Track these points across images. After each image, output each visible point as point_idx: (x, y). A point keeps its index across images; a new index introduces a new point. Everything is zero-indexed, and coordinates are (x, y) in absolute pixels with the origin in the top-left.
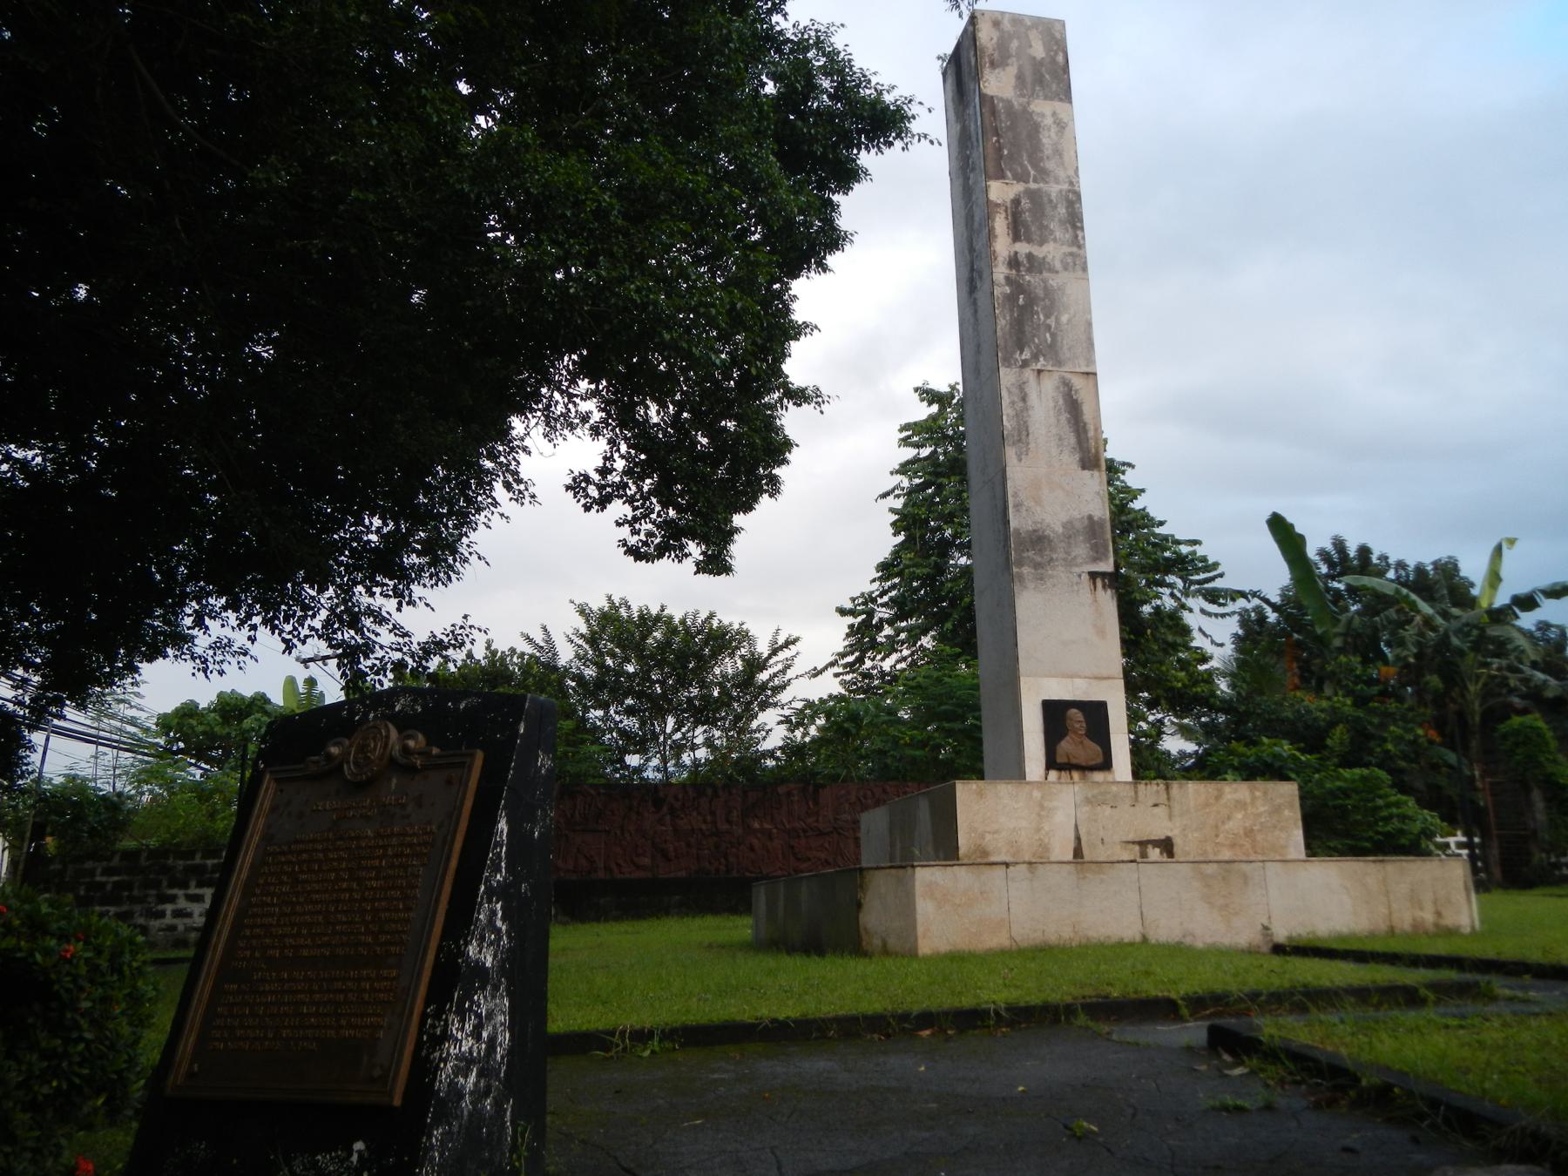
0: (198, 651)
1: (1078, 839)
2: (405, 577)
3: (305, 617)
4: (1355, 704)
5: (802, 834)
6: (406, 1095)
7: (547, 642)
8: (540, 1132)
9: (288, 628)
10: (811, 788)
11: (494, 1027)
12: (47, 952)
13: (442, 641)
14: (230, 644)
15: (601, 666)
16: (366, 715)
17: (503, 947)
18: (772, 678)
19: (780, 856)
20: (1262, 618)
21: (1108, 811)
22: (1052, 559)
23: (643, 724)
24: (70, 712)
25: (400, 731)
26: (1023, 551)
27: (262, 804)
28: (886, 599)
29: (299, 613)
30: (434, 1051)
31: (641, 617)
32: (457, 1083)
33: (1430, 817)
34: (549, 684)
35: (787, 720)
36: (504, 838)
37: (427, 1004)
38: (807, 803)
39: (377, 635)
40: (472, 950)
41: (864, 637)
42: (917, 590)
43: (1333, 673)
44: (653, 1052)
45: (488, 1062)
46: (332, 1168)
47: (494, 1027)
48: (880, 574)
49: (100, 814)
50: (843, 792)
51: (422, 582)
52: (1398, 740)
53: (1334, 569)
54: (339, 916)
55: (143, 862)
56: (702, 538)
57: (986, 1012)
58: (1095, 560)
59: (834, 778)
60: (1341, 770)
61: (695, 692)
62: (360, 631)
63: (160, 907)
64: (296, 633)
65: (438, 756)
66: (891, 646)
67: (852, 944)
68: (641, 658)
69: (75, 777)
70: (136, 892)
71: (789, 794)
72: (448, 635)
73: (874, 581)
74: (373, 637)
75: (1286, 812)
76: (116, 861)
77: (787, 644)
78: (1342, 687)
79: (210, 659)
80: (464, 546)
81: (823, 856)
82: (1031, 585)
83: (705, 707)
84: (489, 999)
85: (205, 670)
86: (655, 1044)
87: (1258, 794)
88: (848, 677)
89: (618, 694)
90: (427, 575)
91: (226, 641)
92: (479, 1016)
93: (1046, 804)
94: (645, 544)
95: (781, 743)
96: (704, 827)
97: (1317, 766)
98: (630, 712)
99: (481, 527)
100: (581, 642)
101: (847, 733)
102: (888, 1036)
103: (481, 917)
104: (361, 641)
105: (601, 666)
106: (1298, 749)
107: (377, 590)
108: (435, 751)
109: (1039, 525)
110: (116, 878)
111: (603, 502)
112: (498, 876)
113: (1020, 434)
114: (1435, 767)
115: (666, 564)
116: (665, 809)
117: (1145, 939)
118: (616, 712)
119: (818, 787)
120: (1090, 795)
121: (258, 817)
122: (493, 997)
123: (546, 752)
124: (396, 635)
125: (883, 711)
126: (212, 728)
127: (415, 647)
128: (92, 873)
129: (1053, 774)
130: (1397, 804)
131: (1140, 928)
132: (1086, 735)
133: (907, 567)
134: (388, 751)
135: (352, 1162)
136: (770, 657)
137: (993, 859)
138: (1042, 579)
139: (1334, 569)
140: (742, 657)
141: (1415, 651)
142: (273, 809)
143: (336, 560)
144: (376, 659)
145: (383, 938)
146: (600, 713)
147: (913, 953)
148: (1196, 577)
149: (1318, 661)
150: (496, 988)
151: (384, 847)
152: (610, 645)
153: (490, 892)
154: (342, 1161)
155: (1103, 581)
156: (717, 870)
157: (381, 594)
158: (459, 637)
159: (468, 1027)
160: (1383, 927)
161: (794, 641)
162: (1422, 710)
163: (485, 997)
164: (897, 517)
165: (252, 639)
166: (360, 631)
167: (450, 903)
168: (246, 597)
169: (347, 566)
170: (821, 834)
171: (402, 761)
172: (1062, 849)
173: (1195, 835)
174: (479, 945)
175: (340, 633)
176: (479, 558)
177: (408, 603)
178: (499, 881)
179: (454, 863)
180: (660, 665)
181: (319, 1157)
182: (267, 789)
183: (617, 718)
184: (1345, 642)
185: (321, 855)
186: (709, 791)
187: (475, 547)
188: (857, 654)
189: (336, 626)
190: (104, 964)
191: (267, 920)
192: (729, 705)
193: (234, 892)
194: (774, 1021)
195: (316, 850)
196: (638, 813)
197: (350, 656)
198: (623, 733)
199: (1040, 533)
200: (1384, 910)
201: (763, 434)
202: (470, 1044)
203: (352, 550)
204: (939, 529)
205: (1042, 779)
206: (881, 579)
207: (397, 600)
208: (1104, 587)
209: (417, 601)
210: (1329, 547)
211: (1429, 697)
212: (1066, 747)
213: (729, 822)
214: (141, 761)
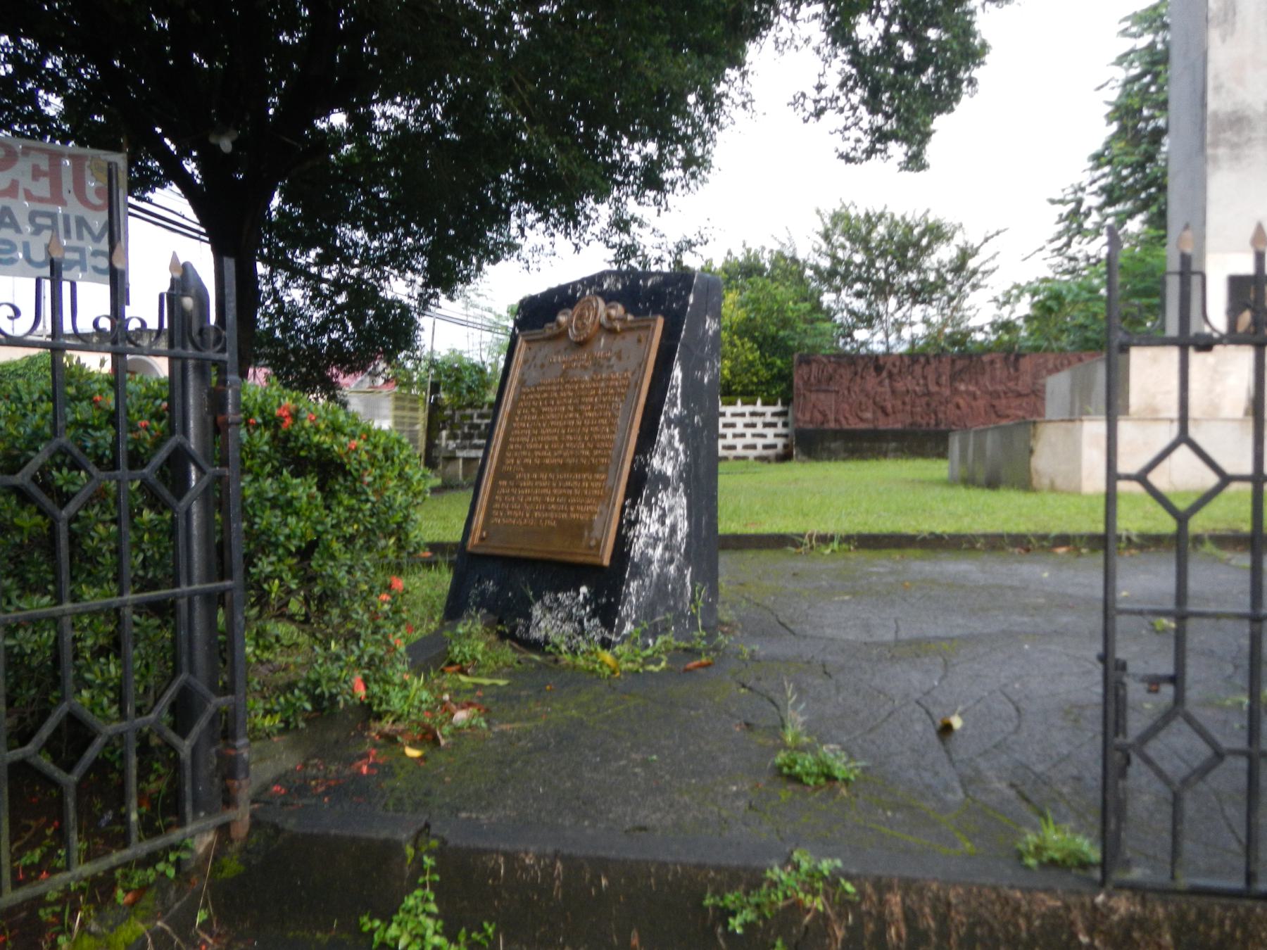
6: (613, 558)
8: (714, 591)
10: (1012, 358)
12: (341, 445)
15: (834, 257)
23: (869, 305)
28: (1095, 187)
35: (996, 300)
37: (626, 499)
41: (1074, 221)
42: (1125, 178)
44: (833, 551)
47: (675, 517)
59: (1037, 349)
65: (632, 322)
67: (1025, 484)
68: (867, 250)
71: (992, 362)
83: (922, 290)
86: (835, 545)
89: (848, 280)
92: (663, 509)
94: (854, 149)
96: (917, 389)
98: (859, 295)
101: (1050, 310)
105: (834, 257)
108: (630, 317)
111: (819, 113)
113: (1226, 14)
116: (884, 374)
119: (1019, 356)
122: (674, 496)
123: (713, 317)
128: (471, 417)
142: (525, 362)
145: (596, 453)
146: (833, 296)
147: (1077, 492)
150: (676, 490)
151: (597, 389)
152: (842, 239)
156: (928, 424)
159: (655, 515)
167: (641, 428)
170: (1019, 395)
171: (607, 325)
180: (883, 254)
186: (922, 360)
190: (379, 453)
191: (523, 439)
192: (943, 287)
194: (932, 534)
196: (862, 377)
198: (852, 313)
201: (962, 39)
204: (1153, 117)
213: (938, 384)
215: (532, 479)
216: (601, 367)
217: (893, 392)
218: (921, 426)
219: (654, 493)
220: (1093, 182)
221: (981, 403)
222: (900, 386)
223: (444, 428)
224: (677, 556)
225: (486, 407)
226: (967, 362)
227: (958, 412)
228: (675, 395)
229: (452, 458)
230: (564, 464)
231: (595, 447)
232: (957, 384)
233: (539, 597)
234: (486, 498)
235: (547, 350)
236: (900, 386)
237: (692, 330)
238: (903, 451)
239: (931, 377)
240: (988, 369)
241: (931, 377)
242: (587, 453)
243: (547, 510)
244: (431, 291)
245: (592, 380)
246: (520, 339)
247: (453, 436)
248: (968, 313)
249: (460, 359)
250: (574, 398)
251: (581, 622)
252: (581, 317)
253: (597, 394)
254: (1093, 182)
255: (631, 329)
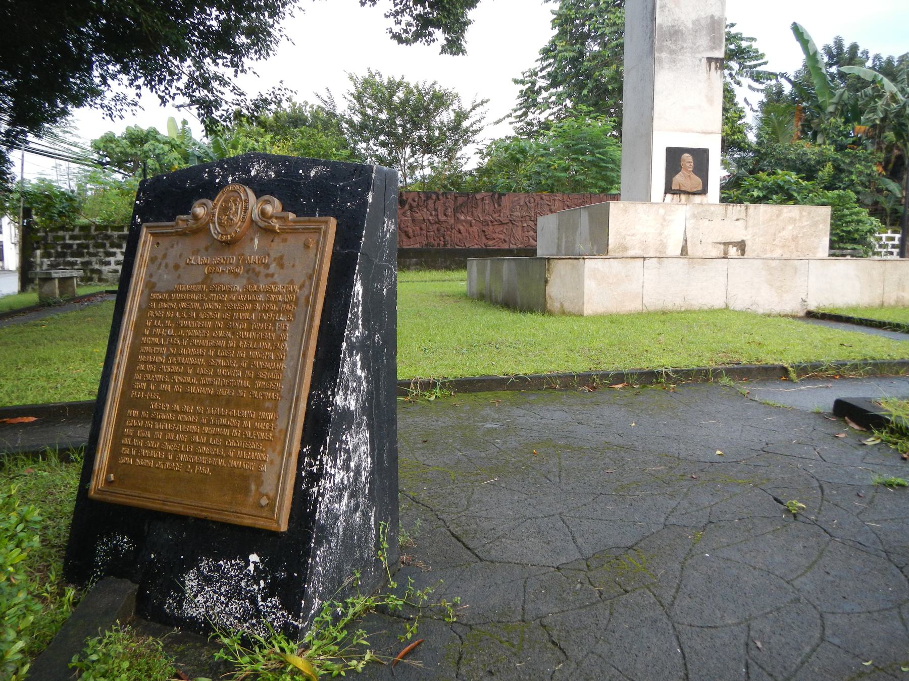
0: (106, 102)
1: (686, 240)
2: (237, 52)
3: (171, 81)
4: (836, 150)
5: (490, 223)
7: (329, 98)
9: (162, 88)
10: (496, 196)
11: (360, 457)
13: (266, 99)
14: (125, 98)
15: (364, 114)
16: (225, 178)
17: (363, 391)
18: (472, 125)
19: (477, 236)
20: (780, 92)
21: (706, 222)
22: (682, 47)
23: (390, 153)
24: (30, 137)
25: (258, 196)
26: (663, 41)
27: (142, 256)
28: (544, 73)
29: (168, 78)
30: (312, 486)
31: (390, 82)
32: (333, 509)
33: (875, 221)
34: (332, 125)
35: (481, 152)
36: (360, 299)
37: (303, 445)
38: (494, 205)
39: (222, 93)
40: (339, 400)
41: (530, 98)
43: (825, 129)
45: (355, 486)
46: (232, 573)
47: (360, 457)
48: (542, 56)
49: (63, 203)
50: (516, 199)
51: (250, 56)
52: (860, 173)
53: (833, 59)
54: (219, 361)
55: (93, 232)
56: (447, 30)
57: (659, 374)
58: (712, 48)
59: (509, 188)
60: (826, 191)
61: (424, 132)
62: (211, 91)
63: (107, 259)
64: (167, 92)
66: (547, 104)
69: (43, 180)
70: (91, 250)
71: (483, 199)
72: (270, 95)
73: (537, 60)
74: (219, 94)
75: (821, 226)
76: (77, 232)
77: (482, 103)
78: (829, 138)
79: (113, 108)
80: (277, 30)
81: (502, 237)
82: (666, 66)
84: (354, 436)
85: (111, 116)
87: (804, 214)
88: (519, 125)
89: (375, 132)
90: (253, 51)
91: (122, 96)
92: (347, 451)
93: (667, 217)
94: (406, 31)
95: (476, 167)
96: (430, 218)
97: (811, 188)
98: (383, 144)
99: (288, 16)
100: (351, 98)
102: (594, 388)
103: (345, 370)
104: (212, 98)
105: (364, 114)
106: (801, 178)
107: (220, 61)
108: (292, 216)
109: (676, 22)
110: (78, 242)
112: (357, 332)
114: (879, 191)
115: (419, 46)
116: (407, 207)
117: (727, 307)
118: (375, 145)
120: (696, 212)
121: (140, 267)
124: (235, 93)
125: (541, 148)
126: (125, 149)
127: (249, 103)
128: (64, 238)
129: (669, 196)
130: (857, 214)
131: (725, 299)
132: (693, 171)
133: (560, 52)
134: (248, 215)
135: (250, 571)
136: (471, 111)
137: (631, 253)
138: (675, 62)
139: (833, 59)
140: (454, 110)
141: (882, 116)
142: (153, 260)
143: (189, 39)
144: (223, 110)
145: (259, 384)
146: (364, 145)
148: (748, 64)
149: (816, 121)
150: (359, 425)
151: (253, 302)
152: (369, 101)
153: (351, 348)
154: (241, 569)
155: (716, 64)
156: (439, 245)
157: (223, 64)
158: (278, 96)
159: (339, 463)
160: (877, 302)
161: (487, 102)
162: (879, 154)
163: (351, 435)
164: (555, 16)
165: (139, 95)
166: (211, 91)
168: (132, 64)
169: (198, 44)
172: (674, 249)
173: (761, 239)
174: (344, 395)
175: (197, 91)
176: (288, 40)
177: (242, 71)
178: (357, 336)
179: (317, 322)
180: (400, 114)
181: (221, 562)
182: (145, 242)
183: (375, 148)
184: (836, 109)
185: (198, 305)
186: (434, 197)
187: (284, 32)
188: (524, 109)
189: (195, 86)
191: (158, 359)
193: (127, 330)
194: (517, 377)
195: (194, 300)
197: (206, 106)
199: (677, 28)
200: (880, 291)
202: (341, 476)
203: (200, 32)
205: (661, 201)
206: (542, 59)
207: (234, 69)
208: (716, 68)
209: (248, 70)
210: (832, 44)
211: (884, 146)
212: (679, 180)
213: (445, 215)
214: (84, 170)
215: (173, 411)
216: (257, 274)
217: (413, 220)
218: (434, 246)
219: (337, 438)
220: (543, 69)
221: (475, 229)
222: (418, 216)
223: (38, 248)
224: (361, 500)
225: (77, 230)
226: (465, 199)
227: (459, 236)
228: (357, 313)
229: (48, 279)
230: (216, 395)
231: (257, 377)
232: (459, 215)
233: (192, 563)
234: (111, 430)
235: (178, 249)
236: (418, 216)
237: (370, 236)
238: (422, 266)
239: (441, 210)
240: (479, 202)
241: (441, 210)
242: (247, 384)
243: (196, 453)
244: (19, 128)
245: (247, 291)
246: (144, 231)
247: (47, 255)
248: (463, 161)
249: (50, 186)
250: (223, 312)
251: (253, 601)
252: (225, 210)
253: (254, 310)
254: (543, 69)
255: (294, 231)
